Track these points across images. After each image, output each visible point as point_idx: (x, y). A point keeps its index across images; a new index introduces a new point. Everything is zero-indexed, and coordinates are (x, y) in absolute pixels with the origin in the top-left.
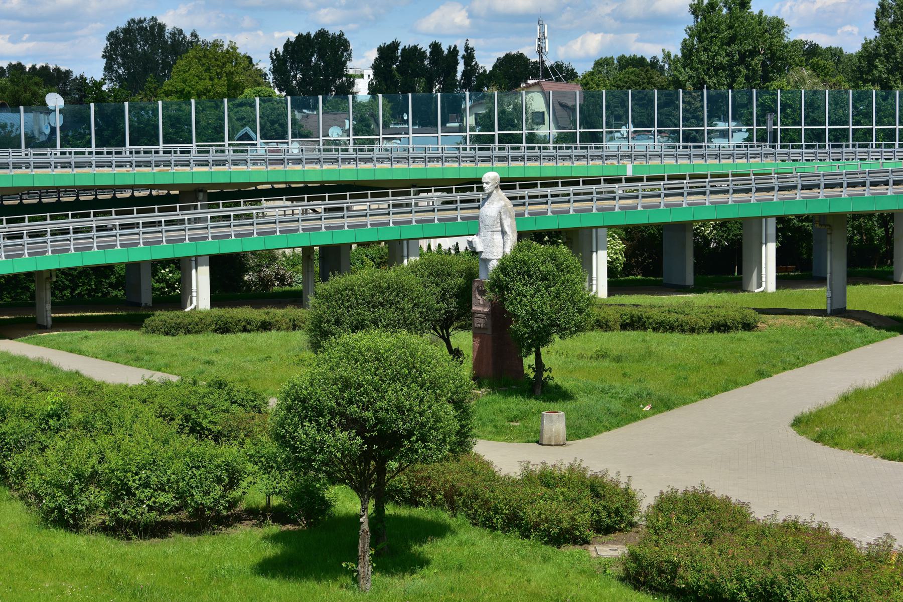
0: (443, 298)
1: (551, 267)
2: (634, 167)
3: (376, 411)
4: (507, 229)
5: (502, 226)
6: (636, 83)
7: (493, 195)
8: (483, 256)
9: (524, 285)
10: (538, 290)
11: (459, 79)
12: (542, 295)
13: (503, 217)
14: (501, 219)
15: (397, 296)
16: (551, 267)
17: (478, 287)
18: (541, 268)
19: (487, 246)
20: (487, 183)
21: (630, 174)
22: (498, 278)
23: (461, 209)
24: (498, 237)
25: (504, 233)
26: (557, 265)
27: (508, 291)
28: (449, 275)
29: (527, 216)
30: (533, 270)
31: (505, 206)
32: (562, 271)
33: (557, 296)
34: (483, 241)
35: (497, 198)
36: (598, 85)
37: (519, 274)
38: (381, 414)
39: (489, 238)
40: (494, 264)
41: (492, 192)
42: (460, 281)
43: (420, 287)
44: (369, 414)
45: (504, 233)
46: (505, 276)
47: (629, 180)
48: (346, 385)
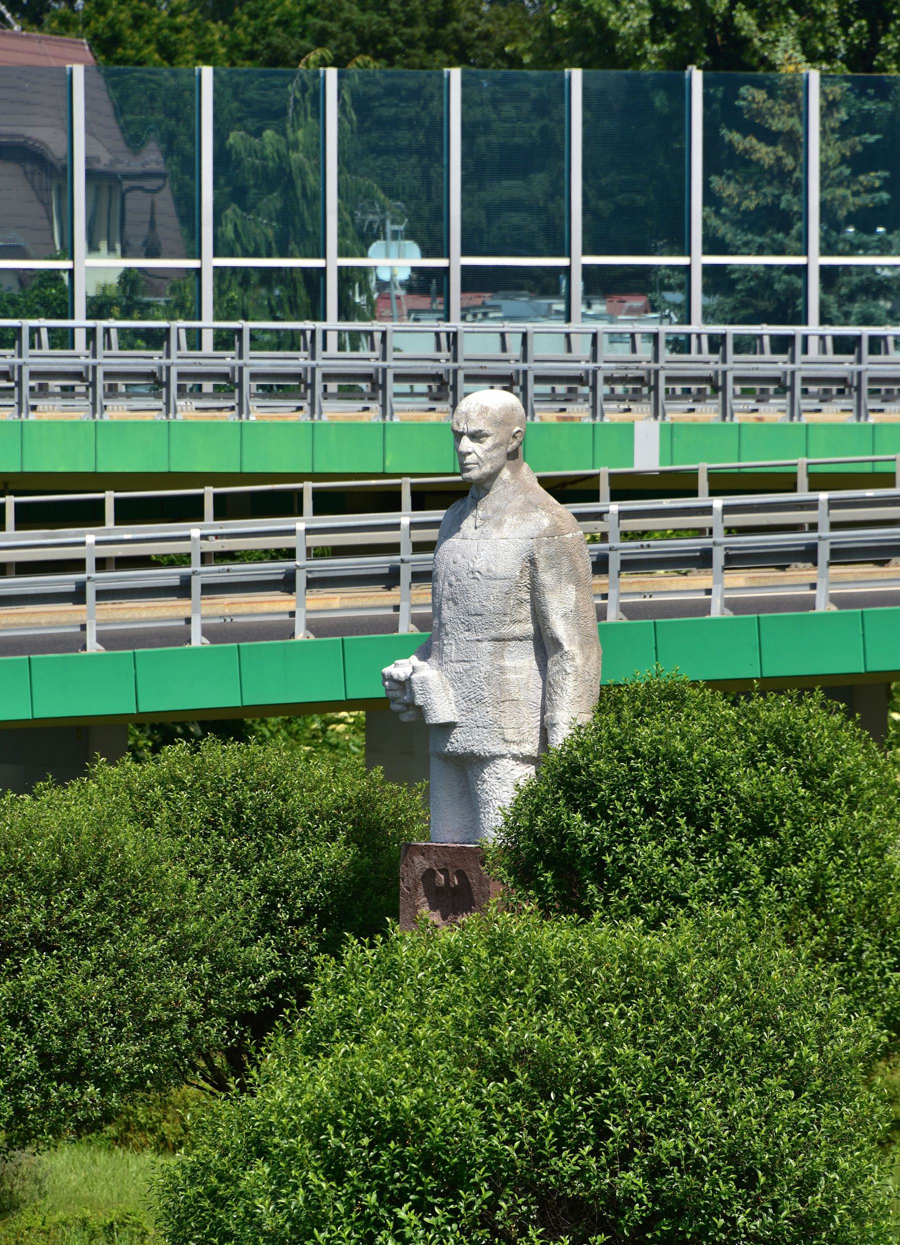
0: (267, 923)
1: (782, 781)
2: (670, 433)
3: (655, 1171)
4: (560, 628)
5: (539, 617)
6: (373, 44)
7: (497, 489)
8: (458, 742)
9: (675, 853)
10: (732, 877)
11: (81, 7)
12: (752, 896)
13: (546, 578)
14: (535, 589)
15: (100, 905)
16: (782, 781)
17: (429, 875)
18: (744, 786)
19: (471, 700)
20: (476, 436)
21: (647, 459)
22: (556, 828)
23: (101, 595)
24: (521, 663)
25: (545, 646)
26: (806, 776)
27: (598, 878)
28: (284, 827)
29: (301, 634)
30: (704, 791)
31: (554, 532)
32: (826, 796)
33: (816, 899)
34: (457, 680)
35: (519, 500)
36: (169, 54)
37: (650, 809)
38: (676, 1182)
39: (484, 666)
40: (505, 786)
41: (492, 477)
42: (336, 854)
43: (177, 873)
44: (631, 1179)
45: (545, 646)
46: (590, 816)
47: (628, 487)
48: (546, 1081)
